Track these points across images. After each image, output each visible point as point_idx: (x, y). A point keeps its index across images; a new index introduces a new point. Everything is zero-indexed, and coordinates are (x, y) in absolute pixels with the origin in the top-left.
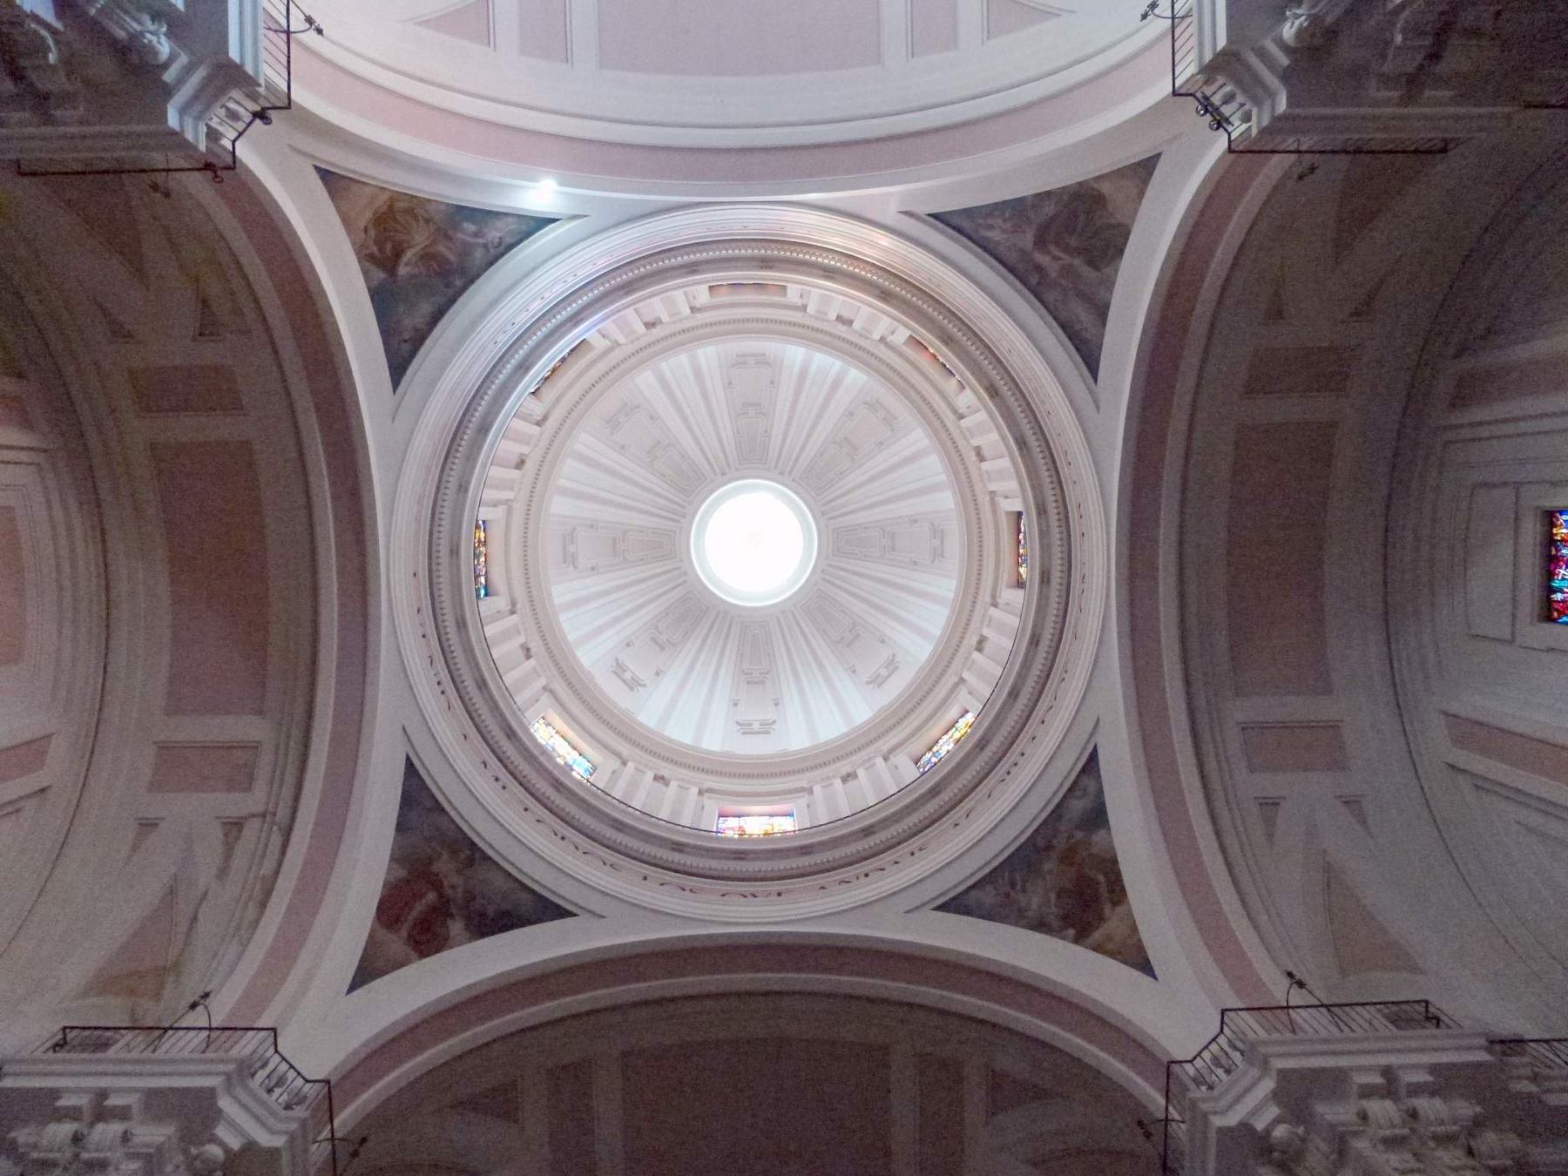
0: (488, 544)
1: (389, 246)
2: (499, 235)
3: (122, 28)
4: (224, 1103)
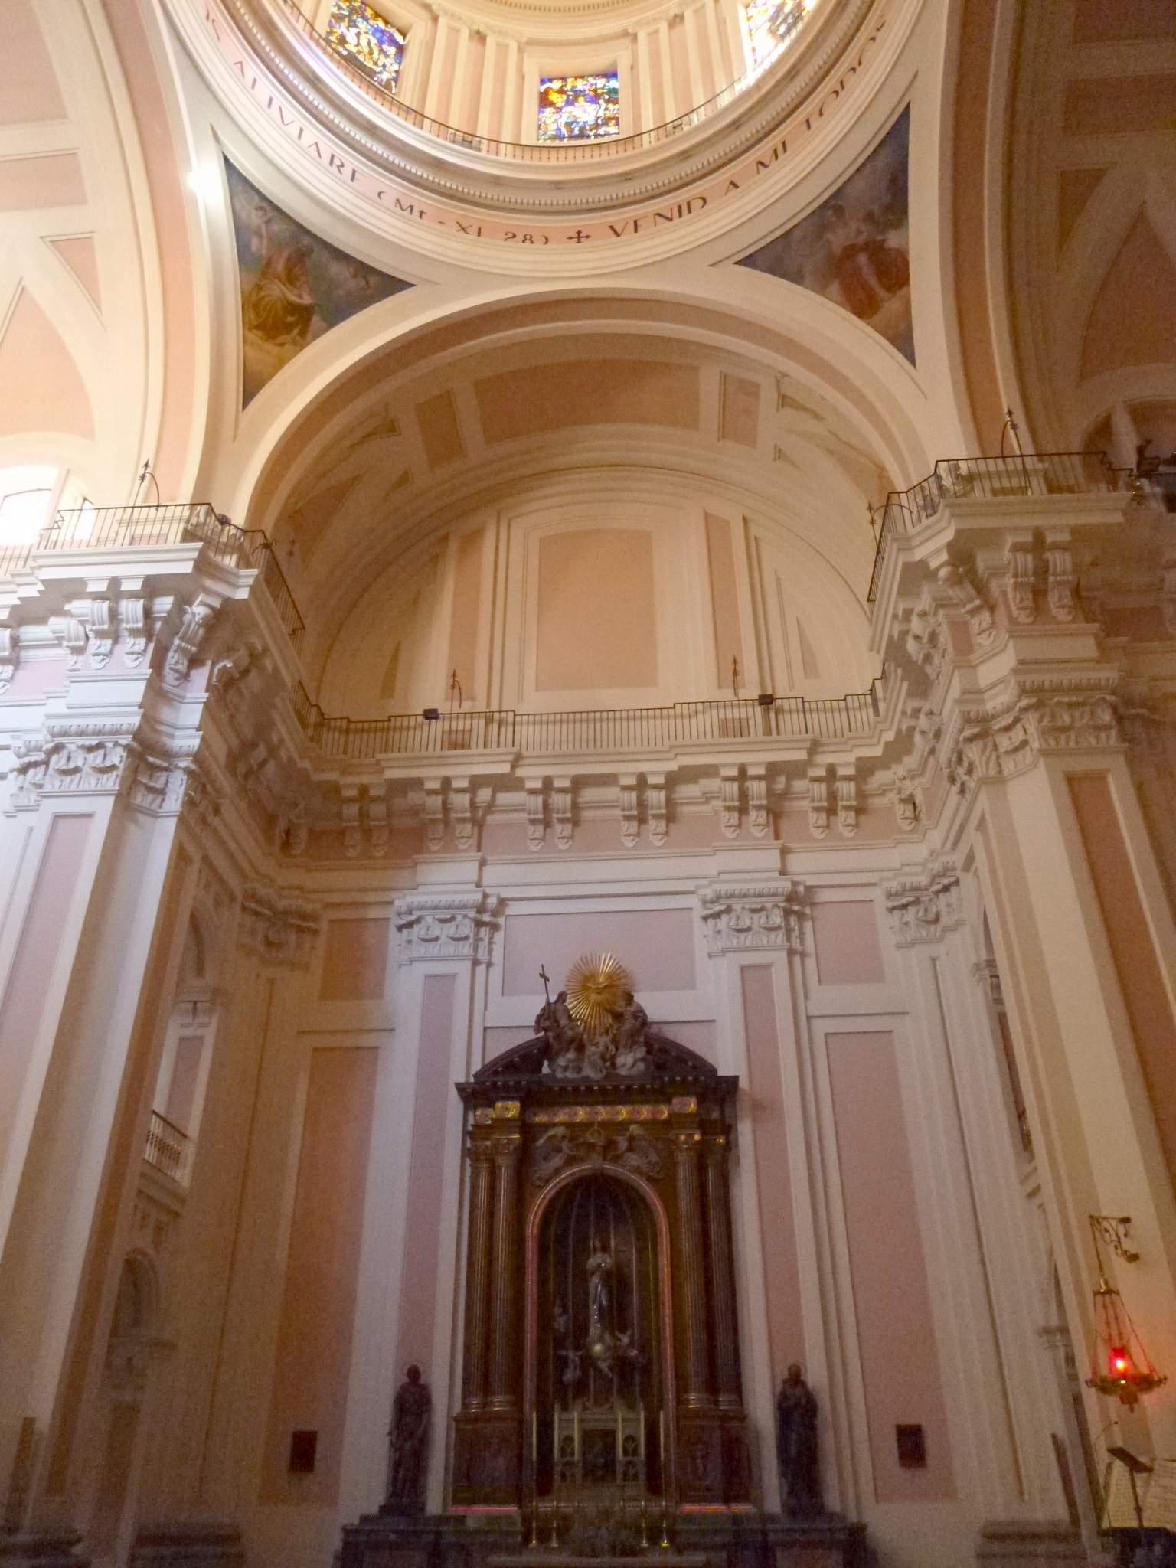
1: (290, 319)
2: (253, 211)
3: (197, 631)
4: (918, 555)
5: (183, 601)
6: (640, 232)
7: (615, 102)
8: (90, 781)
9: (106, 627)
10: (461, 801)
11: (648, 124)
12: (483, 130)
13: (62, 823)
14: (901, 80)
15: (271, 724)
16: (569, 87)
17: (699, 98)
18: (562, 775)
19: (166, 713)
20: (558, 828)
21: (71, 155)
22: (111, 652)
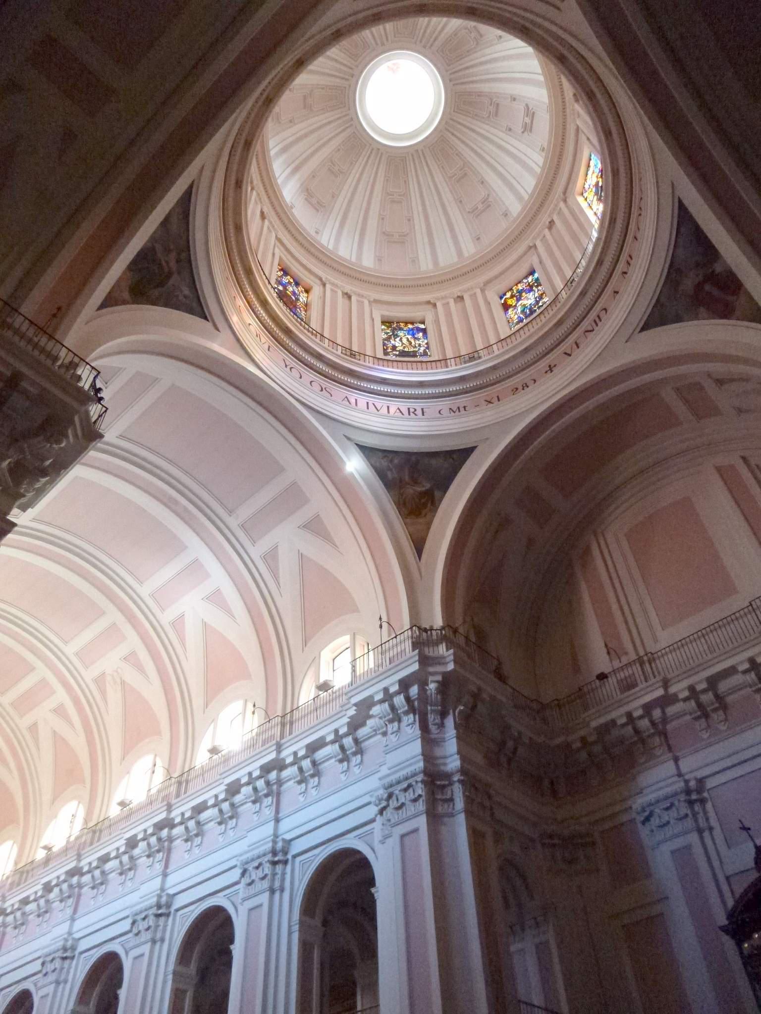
0: (510, 287)
1: (423, 501)
2: (383, 461)
5: (423, 684)
6: (581, 346)
7: (539, 285)
8: (411, 809)
9: (391, 716)
10: (644, 723)
11: (559, 285)
12: (480, 345)
13: (406, 839)
14: (667, 190)
15: (507, 727)
16: (515, 292)
17: (578, 256)
18: (699, 680)
19: (438, 752)
20: (714, 716)
21: (294, 484)
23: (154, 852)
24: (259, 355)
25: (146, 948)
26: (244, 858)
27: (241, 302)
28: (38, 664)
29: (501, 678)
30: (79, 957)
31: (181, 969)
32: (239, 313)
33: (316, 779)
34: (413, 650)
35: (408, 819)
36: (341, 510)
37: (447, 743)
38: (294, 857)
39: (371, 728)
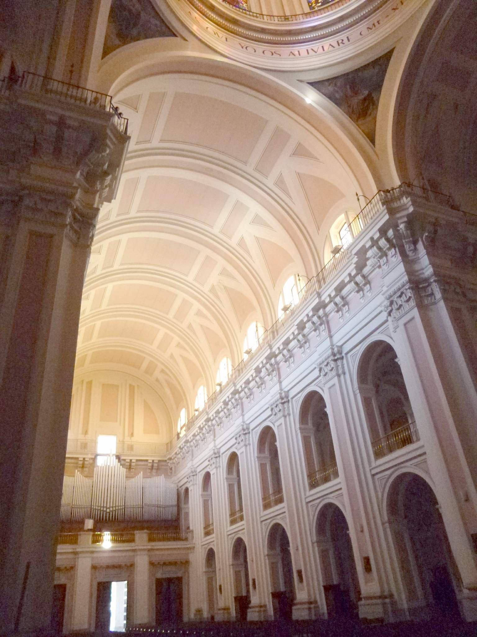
3: (407, 233)
5: (395, 227)
8: (407, 307)
9: (380, 254)
13: (408, 326)
15: (465, 239)
19: (417, 267)
22: (387, 260)
23: (271, 372)
24: (220, 47)
25: (282, 420)
26: (318, 362)
27: (196, 14)
28: (177, 292)
29: (454, 207)
30: (252, 432)
31: (303, 426)
32: (198, 23)
33: (347, 306)
34: (383, 207)
35: (406, 313)
36: (311, 133)
37: (421, 260)
38: (347, 354)
39: (371, 266)
